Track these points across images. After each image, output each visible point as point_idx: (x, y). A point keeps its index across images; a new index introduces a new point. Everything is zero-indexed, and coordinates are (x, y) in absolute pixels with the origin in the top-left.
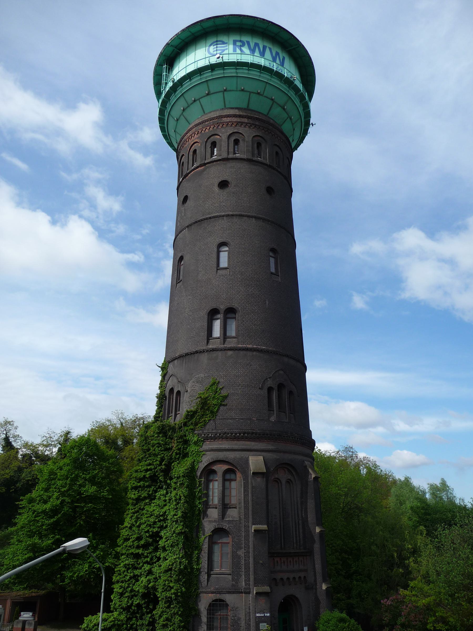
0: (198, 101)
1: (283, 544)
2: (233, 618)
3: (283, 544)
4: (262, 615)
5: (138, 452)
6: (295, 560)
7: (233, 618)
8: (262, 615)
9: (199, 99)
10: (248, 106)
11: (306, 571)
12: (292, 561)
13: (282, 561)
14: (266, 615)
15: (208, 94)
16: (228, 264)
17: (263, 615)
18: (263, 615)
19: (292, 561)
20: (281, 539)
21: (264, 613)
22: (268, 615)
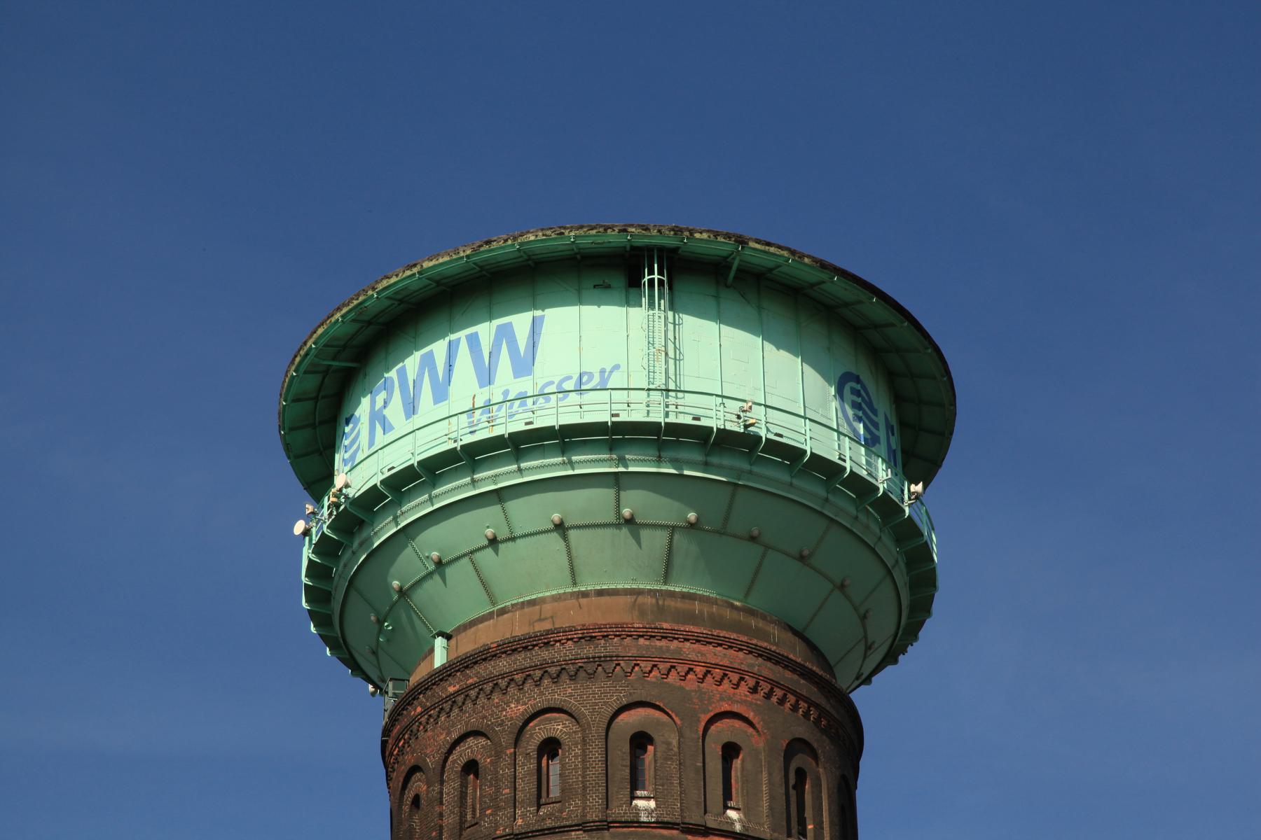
0: (756, 550)
9: (767, 547)
15: (802, 558)
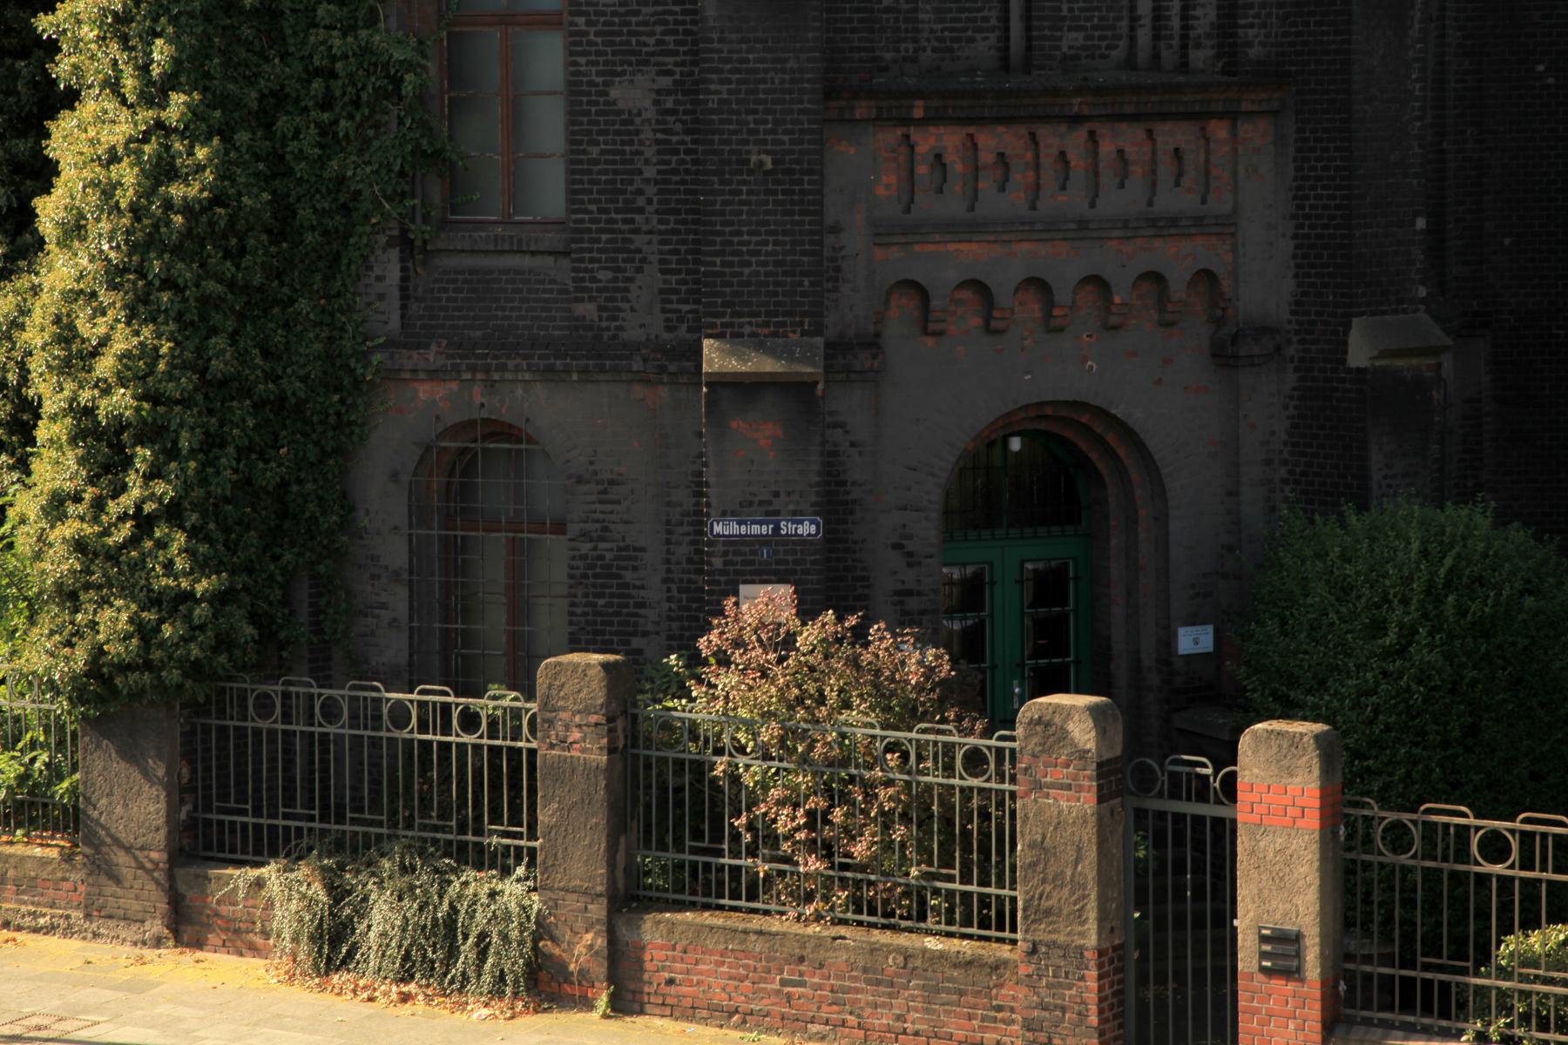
1: (1016, 25)
2: (585, 547)
3: (1016, 25)
4: (756, 529)
5: (299, 200)
6: (1107, 148)
7: (585, 547)
8: (756, 529)
10: (1203, 129)
11: (1225, 226)
12: (1076, 158)
13: (987, 157)
14: (787, 528)
16: (781, 581)
17: (765, 530)
18: (765, 530)
19: (1076, 158)
20: (1005, 19)
21: (772, 515)
22: (807, 529)
